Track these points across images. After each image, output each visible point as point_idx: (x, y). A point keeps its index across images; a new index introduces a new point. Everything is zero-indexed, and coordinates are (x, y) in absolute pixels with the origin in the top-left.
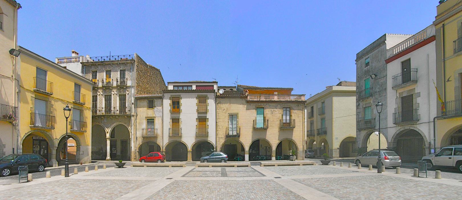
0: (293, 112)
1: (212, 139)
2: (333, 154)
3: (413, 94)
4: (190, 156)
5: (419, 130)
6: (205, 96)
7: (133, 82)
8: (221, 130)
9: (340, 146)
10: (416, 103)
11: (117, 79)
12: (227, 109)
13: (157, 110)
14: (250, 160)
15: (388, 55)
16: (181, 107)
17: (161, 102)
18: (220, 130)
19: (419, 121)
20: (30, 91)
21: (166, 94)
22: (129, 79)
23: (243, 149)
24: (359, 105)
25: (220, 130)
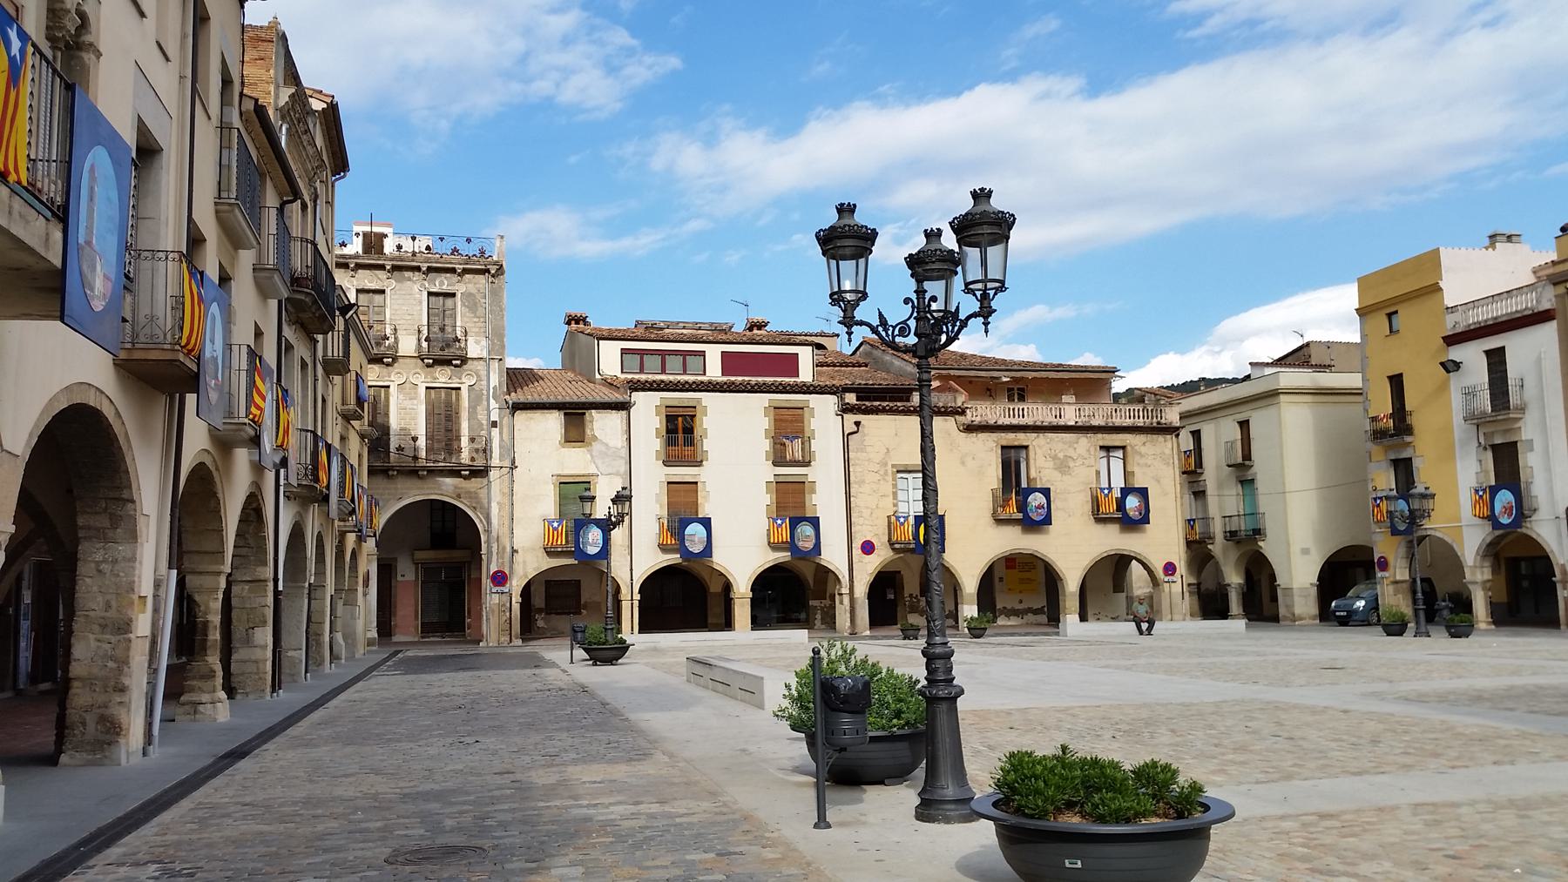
0: (1138, 464)
1: (834, 555)
2: (1296, 604)
3: (1516, 442)
4: (742, 612)
5: (1539, 535)
6: (800, 406)
7: (493, 344)
8: (866, 522)
9: (1319, 579)
10: (1526, 466)
11: (419, 332)
12: (888, 449)
13: (603, 449)
14: (757, 623)
15: (1452, 324)
16: (768, 449)
17: (619, 421)
18: (861, 521)
19: (1537, 512)
20: (1482, 622)
21: (641, 394)
22: (472, 330)
23: (955, 588)
24: (1413, 555)
25: (861, 521)
